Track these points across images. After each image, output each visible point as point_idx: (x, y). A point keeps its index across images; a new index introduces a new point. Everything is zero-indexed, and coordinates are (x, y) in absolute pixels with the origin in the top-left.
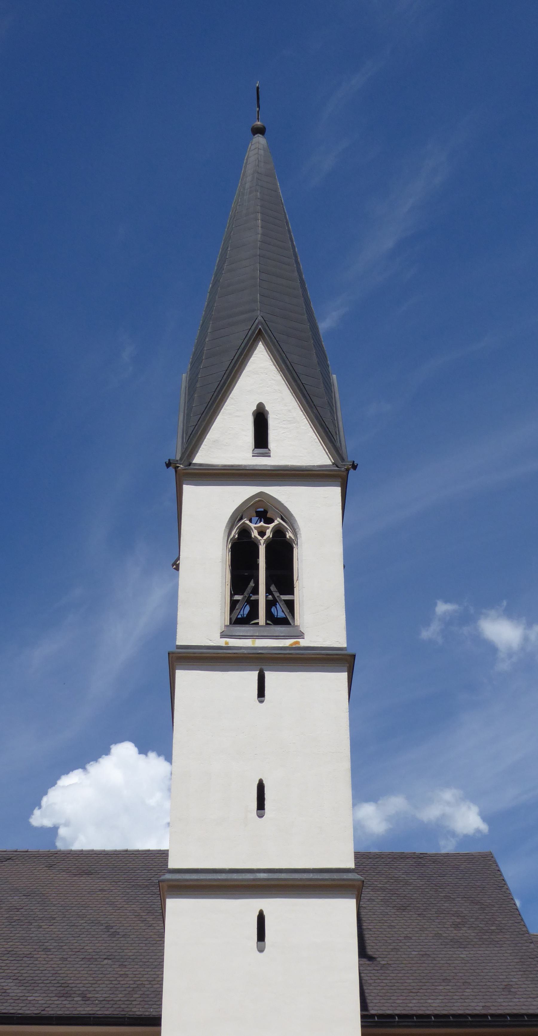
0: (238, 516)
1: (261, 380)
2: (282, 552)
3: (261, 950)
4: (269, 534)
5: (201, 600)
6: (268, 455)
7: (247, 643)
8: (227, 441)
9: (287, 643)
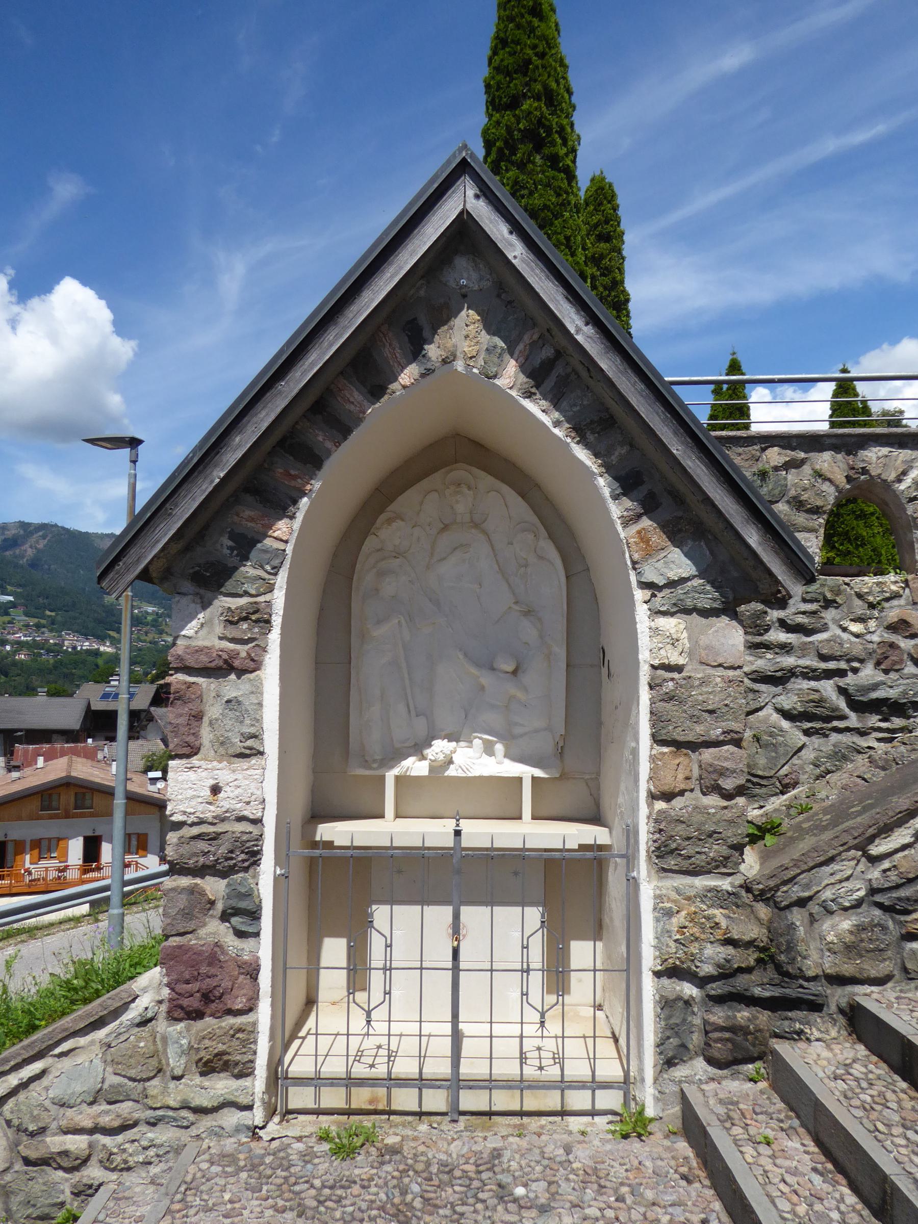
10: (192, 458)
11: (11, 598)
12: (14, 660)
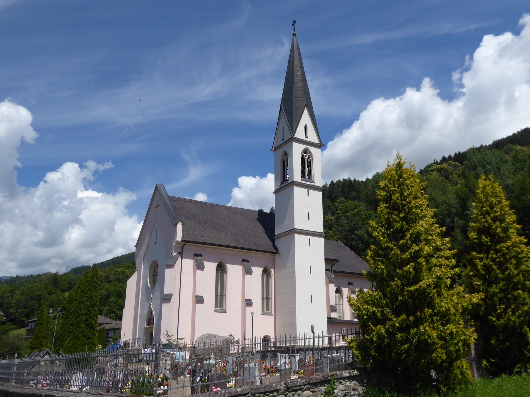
8: (299, 134)
9: (312, 184)
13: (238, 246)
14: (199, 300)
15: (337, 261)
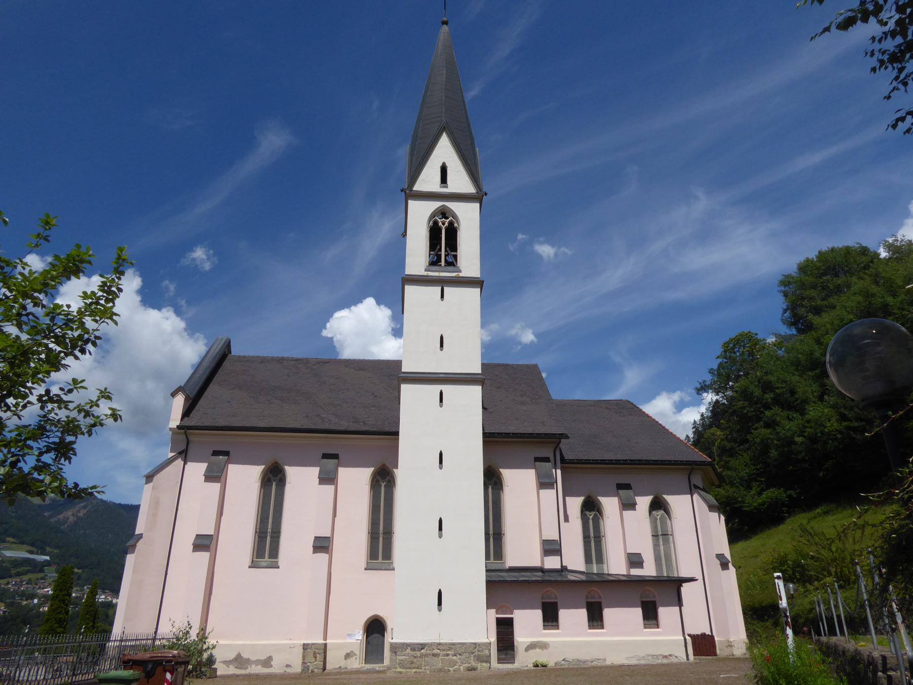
0: (433, 215)
1: (444, 151)
2: (452, 232)
3: (441, 406)
4: (446, 224)
5: (417, 257)
6: (447, 187)
7: (436, 274)
8: (428, 180)
9: (454, 274)
10: (683, 469)
11: (48, 558)
12: (39, 612)
13: (313, 427)
14: (204, 543)
15: (564, 436)
